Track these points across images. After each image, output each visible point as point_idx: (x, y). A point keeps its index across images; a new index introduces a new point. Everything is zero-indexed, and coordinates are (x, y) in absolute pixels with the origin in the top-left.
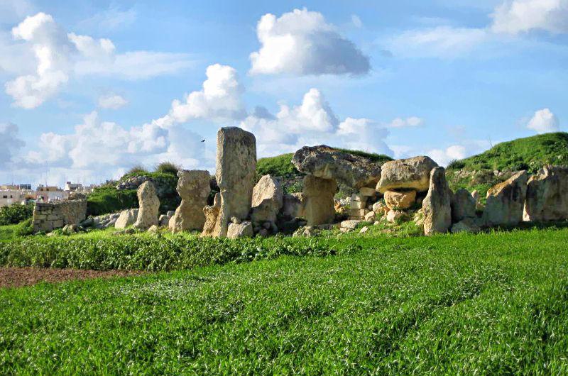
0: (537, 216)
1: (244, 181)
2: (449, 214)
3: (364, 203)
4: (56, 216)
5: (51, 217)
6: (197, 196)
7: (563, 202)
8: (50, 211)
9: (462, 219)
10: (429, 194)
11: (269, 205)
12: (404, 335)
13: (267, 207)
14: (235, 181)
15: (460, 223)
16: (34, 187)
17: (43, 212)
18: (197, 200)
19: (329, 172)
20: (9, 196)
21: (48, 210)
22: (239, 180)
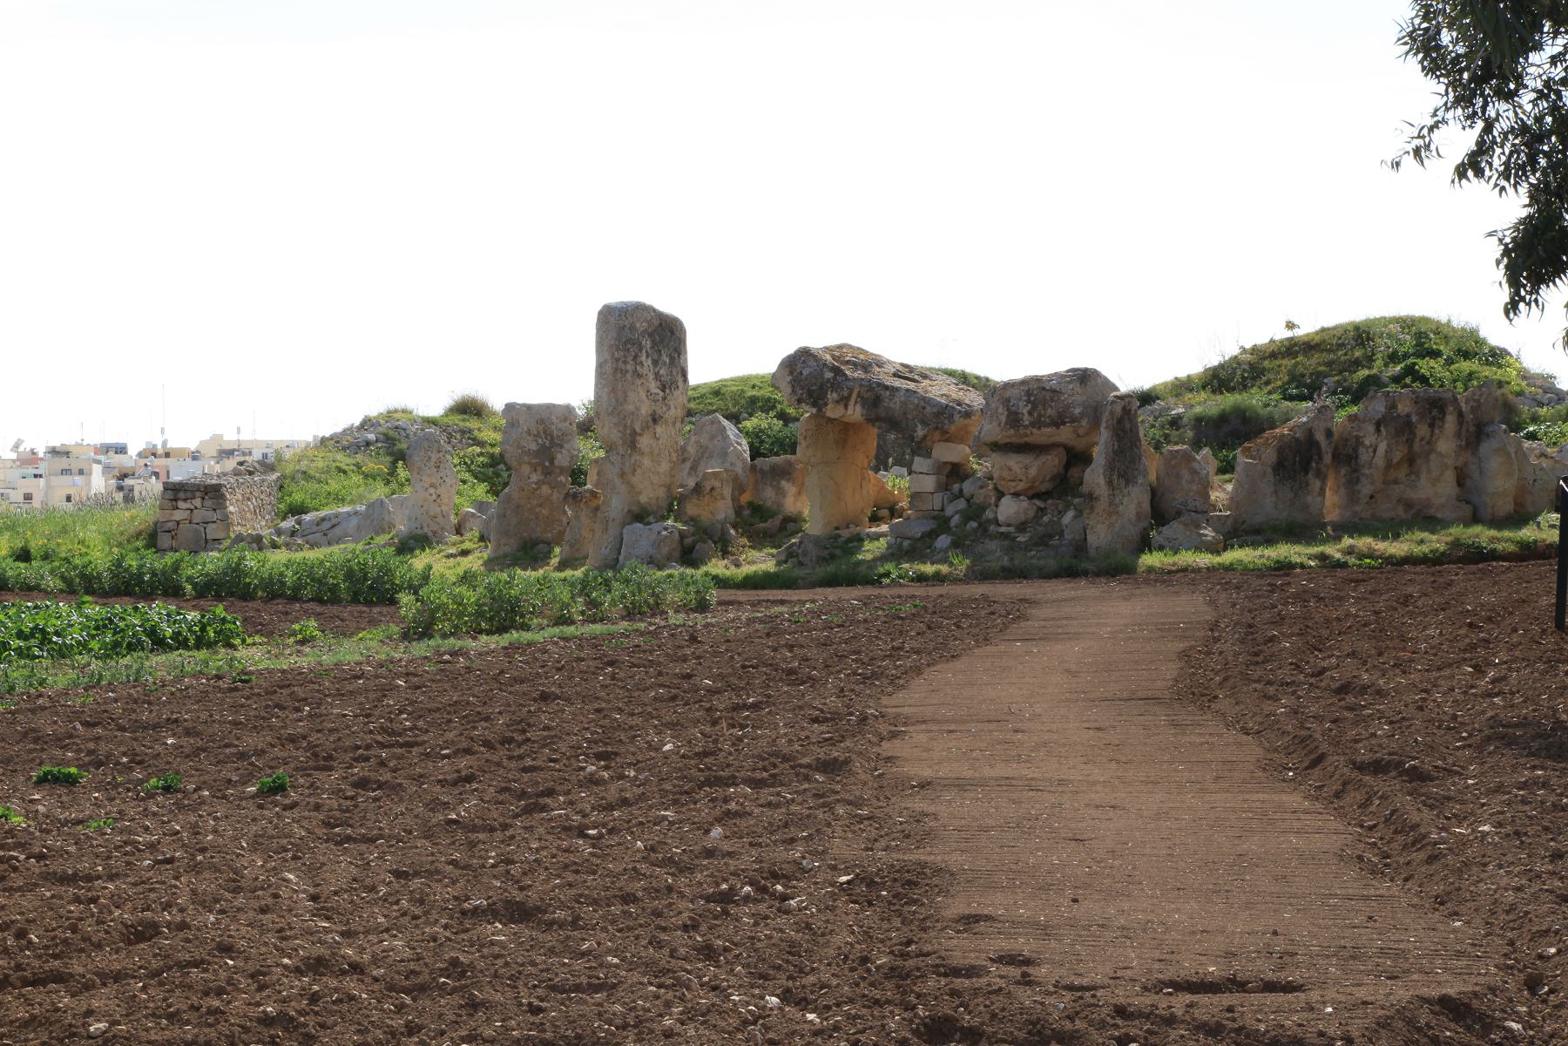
0: (1358, 508)
1: (659, 429)
2: (1146, 506)
3: (943, 478)
4: (210, 513)
5: (199, 516)
6: (547, 464)
7: (1424, 476)
8: (198, 502)
9: (1179, 514)
10: (1320, 549)
11: (717, 484)
12: (1039, 1020)
13: (712, 489)
14: (638, 430)
15: (1174, 524)
16: (133, 451)
17: (181, 504)
18: (547, 472)
19: (858, 408)
20: (75, 470)
21: (194, 498)
22: (648, 427)
